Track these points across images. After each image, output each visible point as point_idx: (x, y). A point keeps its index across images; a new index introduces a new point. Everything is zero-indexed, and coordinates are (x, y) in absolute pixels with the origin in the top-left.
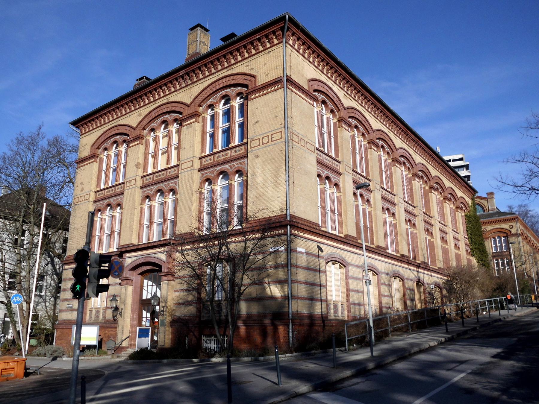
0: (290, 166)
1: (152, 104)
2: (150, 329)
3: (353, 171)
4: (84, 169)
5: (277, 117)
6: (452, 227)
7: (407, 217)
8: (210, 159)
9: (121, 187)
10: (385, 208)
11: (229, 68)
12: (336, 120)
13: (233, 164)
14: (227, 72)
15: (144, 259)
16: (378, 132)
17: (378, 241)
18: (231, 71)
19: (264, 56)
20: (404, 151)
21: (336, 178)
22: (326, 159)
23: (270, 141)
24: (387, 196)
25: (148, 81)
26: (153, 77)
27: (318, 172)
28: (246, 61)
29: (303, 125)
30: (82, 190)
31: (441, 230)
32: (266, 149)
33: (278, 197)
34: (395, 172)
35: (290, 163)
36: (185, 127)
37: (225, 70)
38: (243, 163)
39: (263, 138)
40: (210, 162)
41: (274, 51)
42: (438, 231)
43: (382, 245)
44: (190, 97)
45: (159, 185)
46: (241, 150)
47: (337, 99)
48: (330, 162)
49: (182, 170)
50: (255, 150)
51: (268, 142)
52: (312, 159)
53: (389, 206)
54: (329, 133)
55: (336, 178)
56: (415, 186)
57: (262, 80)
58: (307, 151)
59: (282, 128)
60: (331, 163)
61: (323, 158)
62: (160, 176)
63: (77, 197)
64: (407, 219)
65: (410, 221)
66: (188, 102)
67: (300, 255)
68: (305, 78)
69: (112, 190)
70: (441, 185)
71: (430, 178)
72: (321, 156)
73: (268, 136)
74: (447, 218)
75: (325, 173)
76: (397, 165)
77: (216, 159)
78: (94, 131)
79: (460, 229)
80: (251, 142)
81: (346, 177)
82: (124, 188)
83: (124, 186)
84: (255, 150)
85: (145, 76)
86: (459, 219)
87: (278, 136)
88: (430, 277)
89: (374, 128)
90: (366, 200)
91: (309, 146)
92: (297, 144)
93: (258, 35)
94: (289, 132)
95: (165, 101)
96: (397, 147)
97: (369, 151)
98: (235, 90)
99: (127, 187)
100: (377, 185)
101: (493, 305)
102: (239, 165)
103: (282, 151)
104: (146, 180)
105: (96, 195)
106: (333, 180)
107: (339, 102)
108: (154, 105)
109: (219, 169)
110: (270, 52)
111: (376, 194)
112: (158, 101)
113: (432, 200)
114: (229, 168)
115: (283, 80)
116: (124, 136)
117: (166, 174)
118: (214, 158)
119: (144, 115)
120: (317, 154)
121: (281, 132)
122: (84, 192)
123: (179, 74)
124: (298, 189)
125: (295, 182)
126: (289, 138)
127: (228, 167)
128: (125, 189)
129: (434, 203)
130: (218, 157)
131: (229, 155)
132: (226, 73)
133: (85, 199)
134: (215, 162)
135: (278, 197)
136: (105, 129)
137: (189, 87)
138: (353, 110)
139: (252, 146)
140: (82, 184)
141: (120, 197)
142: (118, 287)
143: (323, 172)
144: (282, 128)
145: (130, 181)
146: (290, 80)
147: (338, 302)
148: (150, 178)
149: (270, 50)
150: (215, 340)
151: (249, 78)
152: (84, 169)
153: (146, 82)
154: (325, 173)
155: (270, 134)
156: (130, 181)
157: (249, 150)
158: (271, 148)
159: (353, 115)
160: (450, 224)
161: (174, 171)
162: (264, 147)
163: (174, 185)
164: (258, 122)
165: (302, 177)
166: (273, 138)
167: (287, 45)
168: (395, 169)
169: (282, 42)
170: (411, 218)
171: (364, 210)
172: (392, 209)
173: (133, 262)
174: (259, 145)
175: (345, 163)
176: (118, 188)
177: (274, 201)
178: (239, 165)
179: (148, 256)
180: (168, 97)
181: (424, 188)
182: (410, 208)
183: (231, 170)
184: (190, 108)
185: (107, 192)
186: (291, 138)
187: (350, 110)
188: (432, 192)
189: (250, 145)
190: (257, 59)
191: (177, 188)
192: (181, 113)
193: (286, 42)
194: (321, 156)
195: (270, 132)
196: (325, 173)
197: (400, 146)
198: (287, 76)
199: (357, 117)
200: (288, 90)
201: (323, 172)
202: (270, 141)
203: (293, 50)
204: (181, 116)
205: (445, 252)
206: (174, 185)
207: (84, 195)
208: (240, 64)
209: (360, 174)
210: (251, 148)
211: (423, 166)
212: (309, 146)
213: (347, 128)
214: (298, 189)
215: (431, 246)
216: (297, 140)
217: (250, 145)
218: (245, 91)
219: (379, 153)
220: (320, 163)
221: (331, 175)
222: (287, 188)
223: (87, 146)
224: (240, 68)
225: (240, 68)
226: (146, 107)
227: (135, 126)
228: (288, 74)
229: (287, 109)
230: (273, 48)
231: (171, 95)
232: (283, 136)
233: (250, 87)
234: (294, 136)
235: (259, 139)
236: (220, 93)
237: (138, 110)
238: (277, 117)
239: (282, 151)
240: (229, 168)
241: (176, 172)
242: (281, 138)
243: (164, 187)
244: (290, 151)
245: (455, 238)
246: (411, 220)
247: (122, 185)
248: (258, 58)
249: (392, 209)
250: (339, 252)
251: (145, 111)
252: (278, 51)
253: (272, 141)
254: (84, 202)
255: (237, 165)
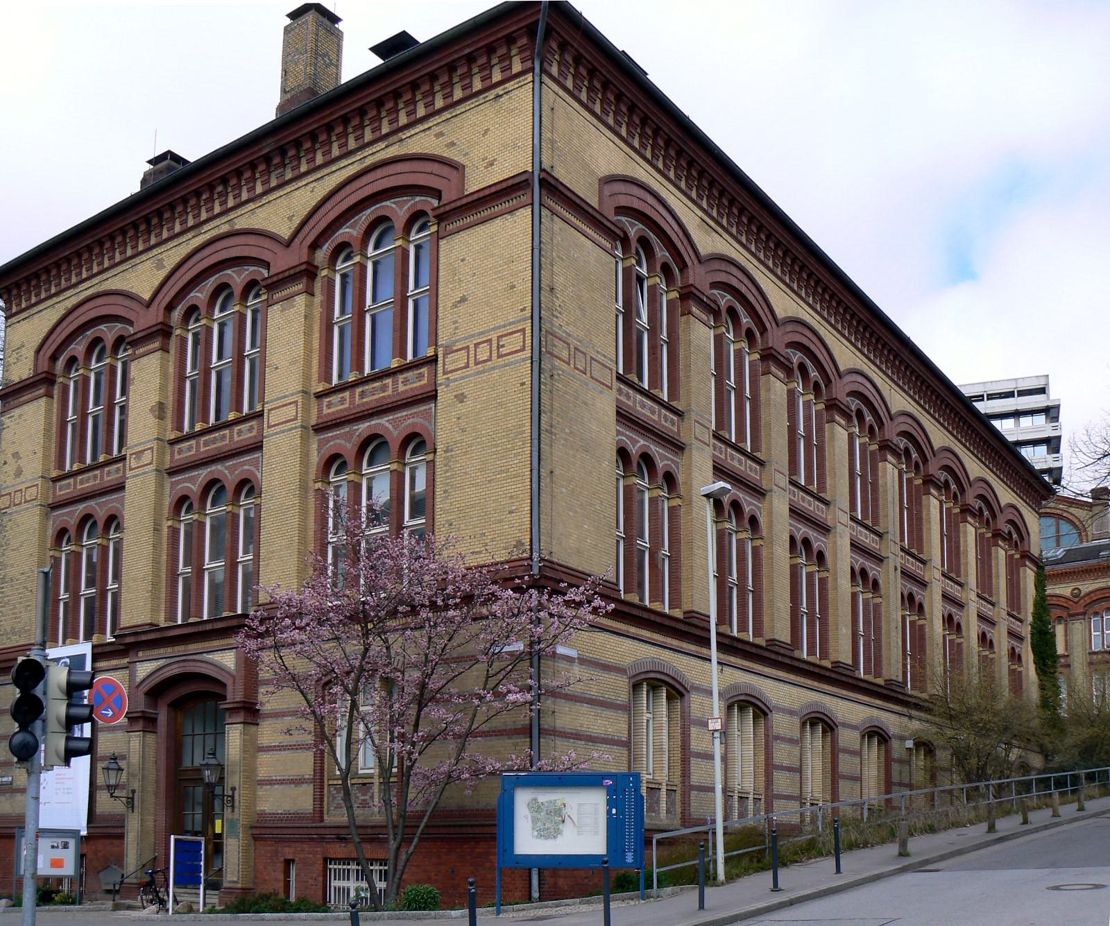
0: (544, 426)
1: (189, 235)
2: (203, 842)
3: (716, 436)
4: (20, 416)
5: (513, 287)
6: (977, 588)
7: (857, 561)
8: (342, 401)
9: (118, 470)
10: (799, 537)
11: (391, 139)
12: (674, 295)
13: (399, 415)
14: (388, 150)
15: (181, 665)
16: (790, 328)
17: (772, 628)
18: (396, 147)
19: (482, 107)
20: (860, 379)
21: (668, 459)
22: (643, 406)
23: (495, 355)
24: (806, 505)
25: (181, 167)
26: (193, 153)
27: (618, 442)
28: (438, 119)
29: (582, 310)
30: (19, 473)
31: (946, 597)
32: (484, 377)
33: (511, 512)
34: (832, 438)
35: (544, 418)
36: (275, 307)
37: (382, 145)
38: (428, 412)
39: (476, 345)
40: (342, 407)
41: (511, 94)
42: (938, 597)
43: (784, 635)
44: (290, 218)
45: (213, 468)
46: (421, 376)
47: (681, 234)
48: (653, 413)
49: (269, 427)
50: (456, 380)
51: (490, 359)
52: (604, 404)
53: (810, 532)
54: (654, 331)
55: (668, 459)
56: (885, 476)
57: (476, 181)
58: (592, 384)
59: (525, 319)
60: (655, 418)
61: (726, 457)
62: (214, 441)
63: (7, 491)
64: (857, 568)
65: (864, 572)
66: (285, 231)
67: (562, 665)
68: (593, 173)
69: (95, 477)
70: (955, 473)
71: (928, 454)
72: (628, 397)
73: (490, 341)
74: (967, 564)
75: (638, 444)
76: (837, 418)
77: (357, 400)
78: (41, 307)
79: (998, 594)
80: (445, 355)
81: (696, 455)
82: (124, 472)
83: (124, 466)
84: (456, 380)
85: (169, 152)
86: (997, 564)
87: (512, 343)
88: (905, 720)
89: (780, 313)
90: (747, 517)
91: (597, 371)
92: (564, 366)
93: (468, 46)
94: (543, 333)
95: (225, 229)
96: (842, 368)
97: (763, 379)
98: (409, 201)
99: (131, 469)
100: (778, 476)
101: (1069, 788)
102: (415, 420)
103: (523, 384)
104: (180, 451)
105: (55, 489)
106: (661, 464)
107: (685, 242)
108: (197, 239)
109: (363, 428)
110: (498, 96)
111: (775, 501)
112: (206, 227)
113: (928, 514)
114: (390, 427)
115: (530, 181)
116: (120, 325)
117: (231, 437)
118: (353, 396)
119: (170, 264)
120: (620, 390)
121: (523, 330)
122: (22, 478)
123: (260, 150)
124: (564, 490)
125: (557, 472)
126: (543, 349)
127: (387, 424)
128: (129, 474)
129: (933, 523)
130: (363, 394)
131: (389, 392)
132: (383, 153)
133: (28, 498)
134: (354, 408)
135: (511, 512)
136: (70, 304)
137: (288, 189)
138: (723, 266)
139: (449, 367)
140: (16, 455)
141: (115, 496)
142: (120, 735)
143: (634, 442)
144: (525, 319)
145: (139, 454)
146: (551, 186)
147: (661, 784)
148: (190, 448)
149: (499, 90)
150: (358, 871)
151: (445, 171)
152: (20, 416)
153: (174, 168)
154: (638, 444)
155: (494, 336)
156: (139, 454)
157: (441, 378)
158: (496, 374)
159: (722, 278)
160: (972, 580)
161: (251, 429)
162: (483, 372)
163: (252, 468)
164: (463, 299)
165: (574, 456)
166: (503, 346)
167: (546, 79)
168: (688, 322)
169: (532, 70)
170: (869, 565)
171: (810, 576)
172: (817, 540)
173: (154, 672)
174: (467, 366)
175: (694, 416)
176: (109, 473)
177: (500, 521)
178: (415, 420)
179: (191, 657)
180: (232, 215)
181: (910, 481)
182: (867, 539)
183: (395, 433)
184: (291, 248)
185: (82, 482)
186: (549, 347)
187: (716, 265)
188: (690, 313)
189: (444, 364)
190: (464, 116)
191: (259, 476)
192: (267, 265)
193: (543, 71)
194: (628, 397)
195: (494, 329)
196: (639, 445)
197: (850, 365)
198: (542, 170)
199: (735, 283)
200: (545, 212)
201: (634, 442)
202: (495, 355)
203: (561, 92)
204: (265, 273)
205: (955, 654)
206: (252, 468)
207: (23, 487)
208: (420, 127)
209: (735, 447)
210: (445, 373)
211: (910, 421)
212: (597, 371)
213: (704, 317)
214: (564, 490)
215: (919, 637)
216: (565, 354)
217: (444, 364)
218: (434, 209)
219: (792, 386)
220: (624, 417)
221: (656, 450)
222: (535, 485)
223: (23, 351)
224: (421, 141)
225: (421, 141)
226: (175, 242)
227: (147, 296)
228: (546, 165)
229: (540, 265)
230: (509, 86)
231: (239, 212)
232: (528, 342)
233: (446, 197)
234: (556, 342)
235: (468, 347)
236: (369, 211)
237: (155, 252)
238: (513, 287)
239: (523, 384)
240: (390, 427)
241: (254, 433)
242: (523, 349)
243: (226, 472)
244: (545, 385)
245: (982, 617)
246: (868, 570)
247: (120, 465)
248: (468, 113)
249: (817, 540)
250: (666, 655)
251: (173, 254)
252: (521, 95)
253: (499, 356)
254: (25, 506)
255: (407, 420)
